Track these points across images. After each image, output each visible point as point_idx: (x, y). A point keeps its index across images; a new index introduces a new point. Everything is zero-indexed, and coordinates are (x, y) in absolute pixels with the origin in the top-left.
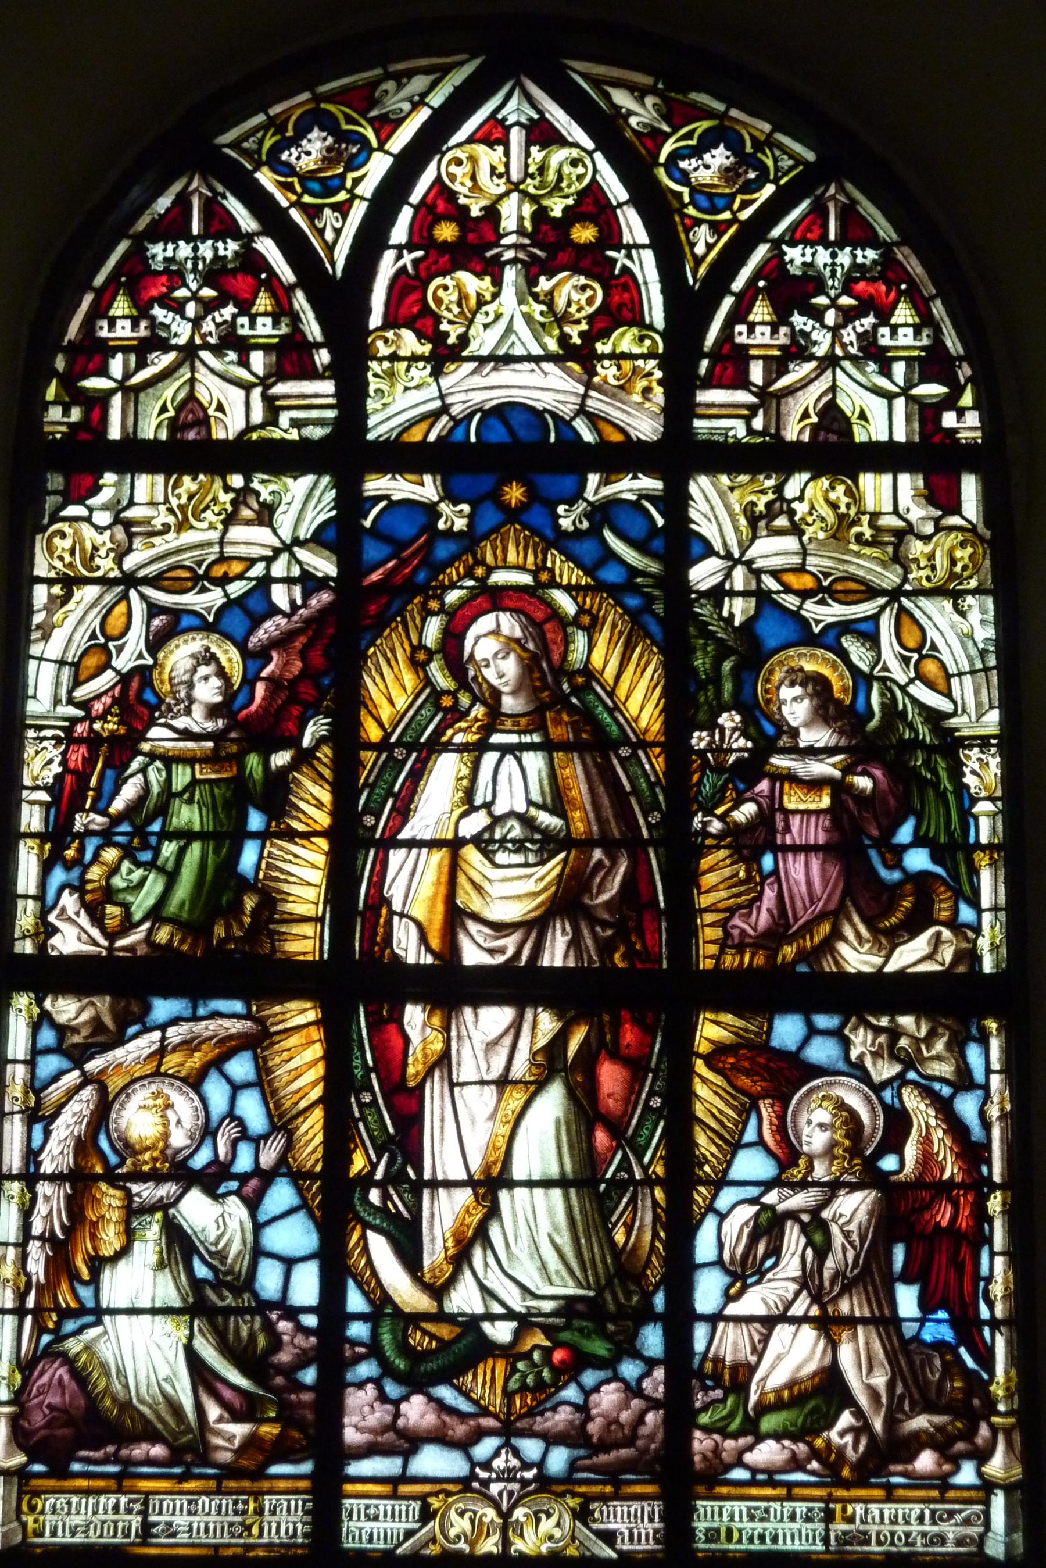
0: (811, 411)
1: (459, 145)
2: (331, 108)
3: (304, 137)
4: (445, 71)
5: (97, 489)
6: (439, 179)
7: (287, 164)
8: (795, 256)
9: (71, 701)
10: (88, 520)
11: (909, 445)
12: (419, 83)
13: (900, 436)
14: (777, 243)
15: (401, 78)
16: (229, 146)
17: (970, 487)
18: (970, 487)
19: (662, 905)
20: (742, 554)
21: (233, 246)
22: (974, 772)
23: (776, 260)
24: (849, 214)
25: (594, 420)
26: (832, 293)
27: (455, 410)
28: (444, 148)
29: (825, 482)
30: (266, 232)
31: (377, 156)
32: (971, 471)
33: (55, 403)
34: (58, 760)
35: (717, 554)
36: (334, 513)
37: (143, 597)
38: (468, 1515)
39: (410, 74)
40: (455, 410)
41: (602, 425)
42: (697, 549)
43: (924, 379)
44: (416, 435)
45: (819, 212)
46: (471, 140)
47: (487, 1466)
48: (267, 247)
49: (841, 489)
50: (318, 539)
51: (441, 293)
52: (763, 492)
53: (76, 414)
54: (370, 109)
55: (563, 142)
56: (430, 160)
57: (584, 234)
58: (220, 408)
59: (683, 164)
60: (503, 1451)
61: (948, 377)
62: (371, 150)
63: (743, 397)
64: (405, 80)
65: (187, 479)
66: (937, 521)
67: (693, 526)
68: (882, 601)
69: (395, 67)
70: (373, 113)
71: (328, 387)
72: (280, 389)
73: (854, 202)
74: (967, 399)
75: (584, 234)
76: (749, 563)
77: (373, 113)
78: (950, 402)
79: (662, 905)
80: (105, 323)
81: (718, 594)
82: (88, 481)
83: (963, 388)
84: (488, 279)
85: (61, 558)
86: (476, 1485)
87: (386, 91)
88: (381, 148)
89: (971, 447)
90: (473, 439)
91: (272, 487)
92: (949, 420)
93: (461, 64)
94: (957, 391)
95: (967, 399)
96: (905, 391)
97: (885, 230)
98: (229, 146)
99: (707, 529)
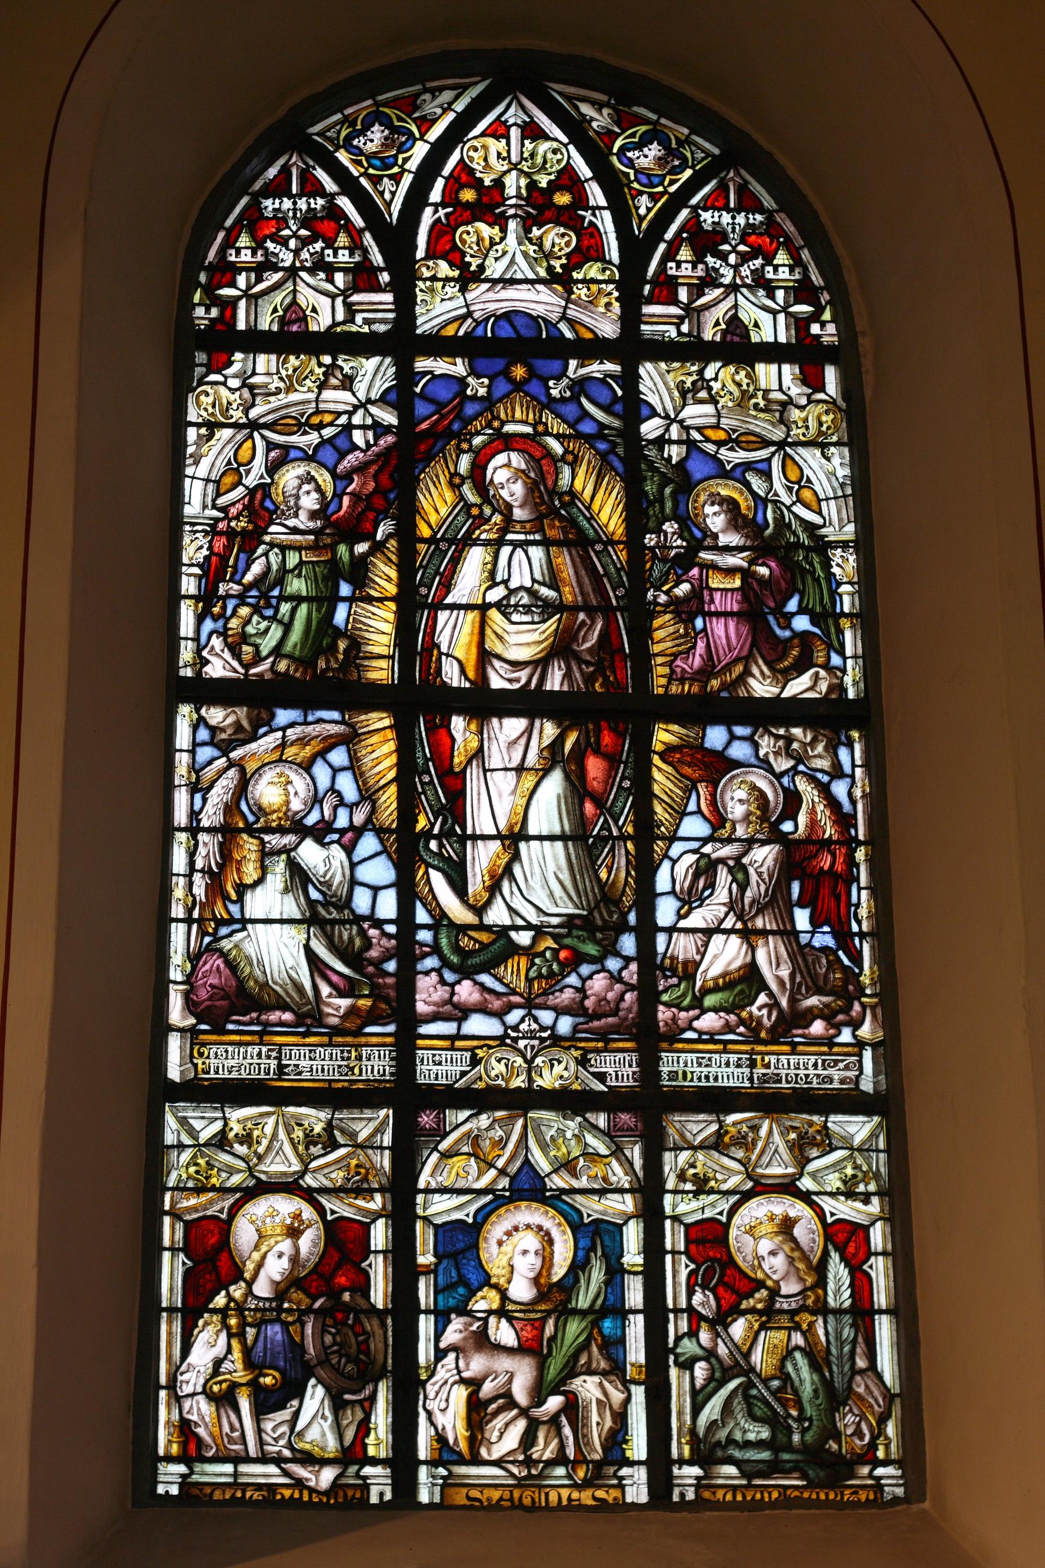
4: (465, 88)
5: (230, 364)
6: (462, 160)
7: (357, 147)
10: (224, 384)
12: (447, 96)
13: (782, 339)
14: (695, 208)
15: (435, 92)
16: (317, 134)
17: (830, 375)
18: (830, 375)
22: (838, 565)
23: (694, 222)
24: (743, 191)
25: (572, 323)
26: (733, 243)
29: (732, 369)
31: (419, 143)
35: (659, 416)
37: (263, 437)
39: (441, 89)
42: (645, 411)
44: (450, 331)
45: (722, 189)
46: (483, 134)
48: (344, 203)
49: (743, 373)
50: (383, 400)
51: (465, 236)
53: (214, 312)
54: (414, 112)
55: (547, 138)
57: (562, 199)
59: (630, 154)
62: (415, 140)
65: (292, 358)
66: (809, 396)
70: (416, 115)
71: (389, 297)
72: (355, 298)
74: (827, 316)
75: (562, 199)
77: (416, 115)
78: (815, 317)
82: (224, 357)
84: (497, 228)
88: (422, 139)
89: (831, 347)
91: (351, 364)
92: (815, 329)
93: (476, 83)
94: (820, 310)
95: (827, 316)
96: (784, 309)
97: (768, 202)
98: (317, 134)
99: (653, 399)
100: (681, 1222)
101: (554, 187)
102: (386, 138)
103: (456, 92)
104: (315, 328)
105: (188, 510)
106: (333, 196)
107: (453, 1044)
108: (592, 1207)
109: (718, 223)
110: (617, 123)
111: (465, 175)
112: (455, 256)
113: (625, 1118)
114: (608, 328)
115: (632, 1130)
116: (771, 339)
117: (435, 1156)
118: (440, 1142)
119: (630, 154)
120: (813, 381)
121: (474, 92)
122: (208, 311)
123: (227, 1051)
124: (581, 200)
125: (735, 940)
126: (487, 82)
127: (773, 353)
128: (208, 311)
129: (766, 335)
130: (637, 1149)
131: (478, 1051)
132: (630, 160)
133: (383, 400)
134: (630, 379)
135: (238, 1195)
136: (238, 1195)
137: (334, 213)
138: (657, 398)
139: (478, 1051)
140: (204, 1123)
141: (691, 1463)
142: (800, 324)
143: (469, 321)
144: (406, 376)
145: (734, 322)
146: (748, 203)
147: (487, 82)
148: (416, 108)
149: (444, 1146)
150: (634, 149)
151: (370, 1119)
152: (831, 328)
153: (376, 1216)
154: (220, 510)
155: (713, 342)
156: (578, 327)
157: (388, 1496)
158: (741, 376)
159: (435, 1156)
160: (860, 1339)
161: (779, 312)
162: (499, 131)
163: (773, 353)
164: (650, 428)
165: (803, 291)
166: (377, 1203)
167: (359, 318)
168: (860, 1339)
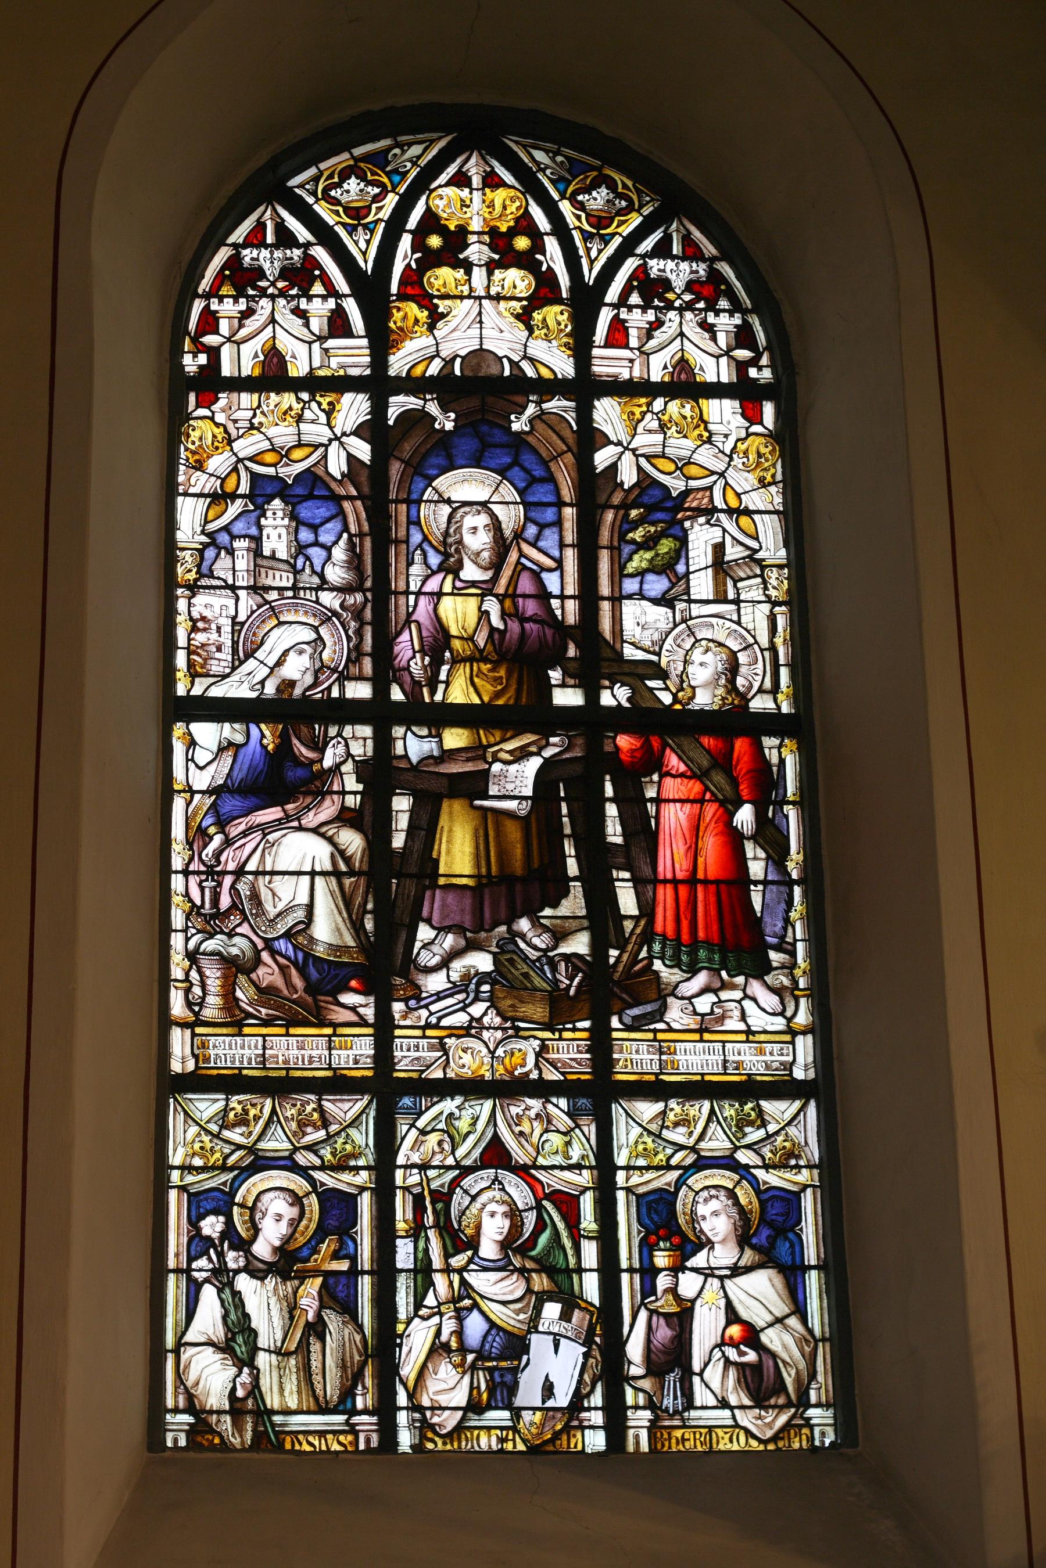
0: (669, 366)
1: (440, 186)
2: (362, 165)
3: (344, 182)
4: (432, 142)
5: (217, 399)
8: (655, 266)
9: (203, 532)
11: (730, 385)
13: (725, 379)
14: (643, 257)
15: (403, 146)
17: (768, 410)
18: (768, 410)
19: (561, 785)
20: (629, 444)
21: (297, 253)
22: (774, 588)
23: (643, 269)
24: (687, 240)
25: (532, 361)
26: (678, 291)
27: (443, 354)
28: (433, 186)
29: (677, 402)
30: (320, 243)
31: (391, 195)
32: (768, 399)
33: (188, 352)
34: (195, 570)
36: (369, 417)
37: (247, 468)
38: (469, 1051)
39: (410, 145)
40: (443, 354)
41: (538, 365)
42: (599, 439)
43: (739, 346)
44: (418, 371)
45: (667, 240)
46: (448, 184)
47: (479, 1020)
48: (320, 253)
50: (357, 432)
51: (432, 280)
52: (640, 406)
53: (203, 359)
56: (424, 193)
57: (522, 243)
58: (294, 357)
60: (489, 1012)
61: (752, 344)
62: (388, 192)
63: (625, 353)
64: (406, 148)
65: (273, 395)
67: (595, 425)
68: (714, 478)
69: (401, 139)
70: (388, 169)
71: (365, 342)
72: (331, 343)
73: (689, 233)
74: (764, 360)
75: (522, 243)
76: (634, 451)
77: (388, 169)
78: (754, 362)
79: (561, 785)
80: (216, 300)
81: (613, 468)
83: (763, 353)
84: (462, 271)
85: (193, 443)
86: (473, 1031)
87: (395, 155)
90: (458, 372)
91: (328, 399)
92: (753, 373)
93: (440, 138)
94: (759, 356)
95: (764, 360)
96: (727, 353)
97: (709, 249)
98: (298, 187)
100: (634, 1193)
101: (513, 232)
102: (361, 191)
103: (424, 146)
104: (295, 375)
105: (180, 536)
106: (308, 245)
107: (424, 1033)
108: (553, 1181)
109: (664, 271)
110: (569, 171)
111: (431, 222)
112: (425, 300)
113: (583, 1102)
114: (564, 366)
115: (411, 1108)
116: (715, 380)
117: (414, 1133)
118: (416, 1119)
119: (580, 198)
120: (752, 416)
121: (442, 144)
122: (195, 356)
123: (224, 1042)
124: (537, 238)
125: (671, 697)
126: (449, 138)
127: (717, 390)
128: (195, 356)
129: (711, 377)
130: (593, 1128)
131: (447, 1040)
132: (582, 203)
133: (357, 432)
134: (585, 414)
135: (236, 1172)
136: (236, 1172)
137: (311, 263)
138: (610, 426)
139: (447, 1040)
140: (207, 1104)
141: (644, 1408)
142: (742, 367)
143: (437, 361)
144: (379, 409)
145: (683, 364)
146: (690, 252)
147: (449, 138)
148: (388, 163)
149: (421, 1123)
150: (584, 193)
151: (357, 1100)
152: (767, 374)
153: (362, 1189)
154: (208, 535)
155: (663, 382)
156: (538, 365)
157: (374, 1443)
158: (687, 411)
159: (414, 1133)
160: (652, 1027)
161: (721, 356)
162: (461, 180)
163: (717, 390)
164: (602, 458)
165: (743, 337)
166: (363, 1178)
167: (334, 362)
168: (652, 1027)
